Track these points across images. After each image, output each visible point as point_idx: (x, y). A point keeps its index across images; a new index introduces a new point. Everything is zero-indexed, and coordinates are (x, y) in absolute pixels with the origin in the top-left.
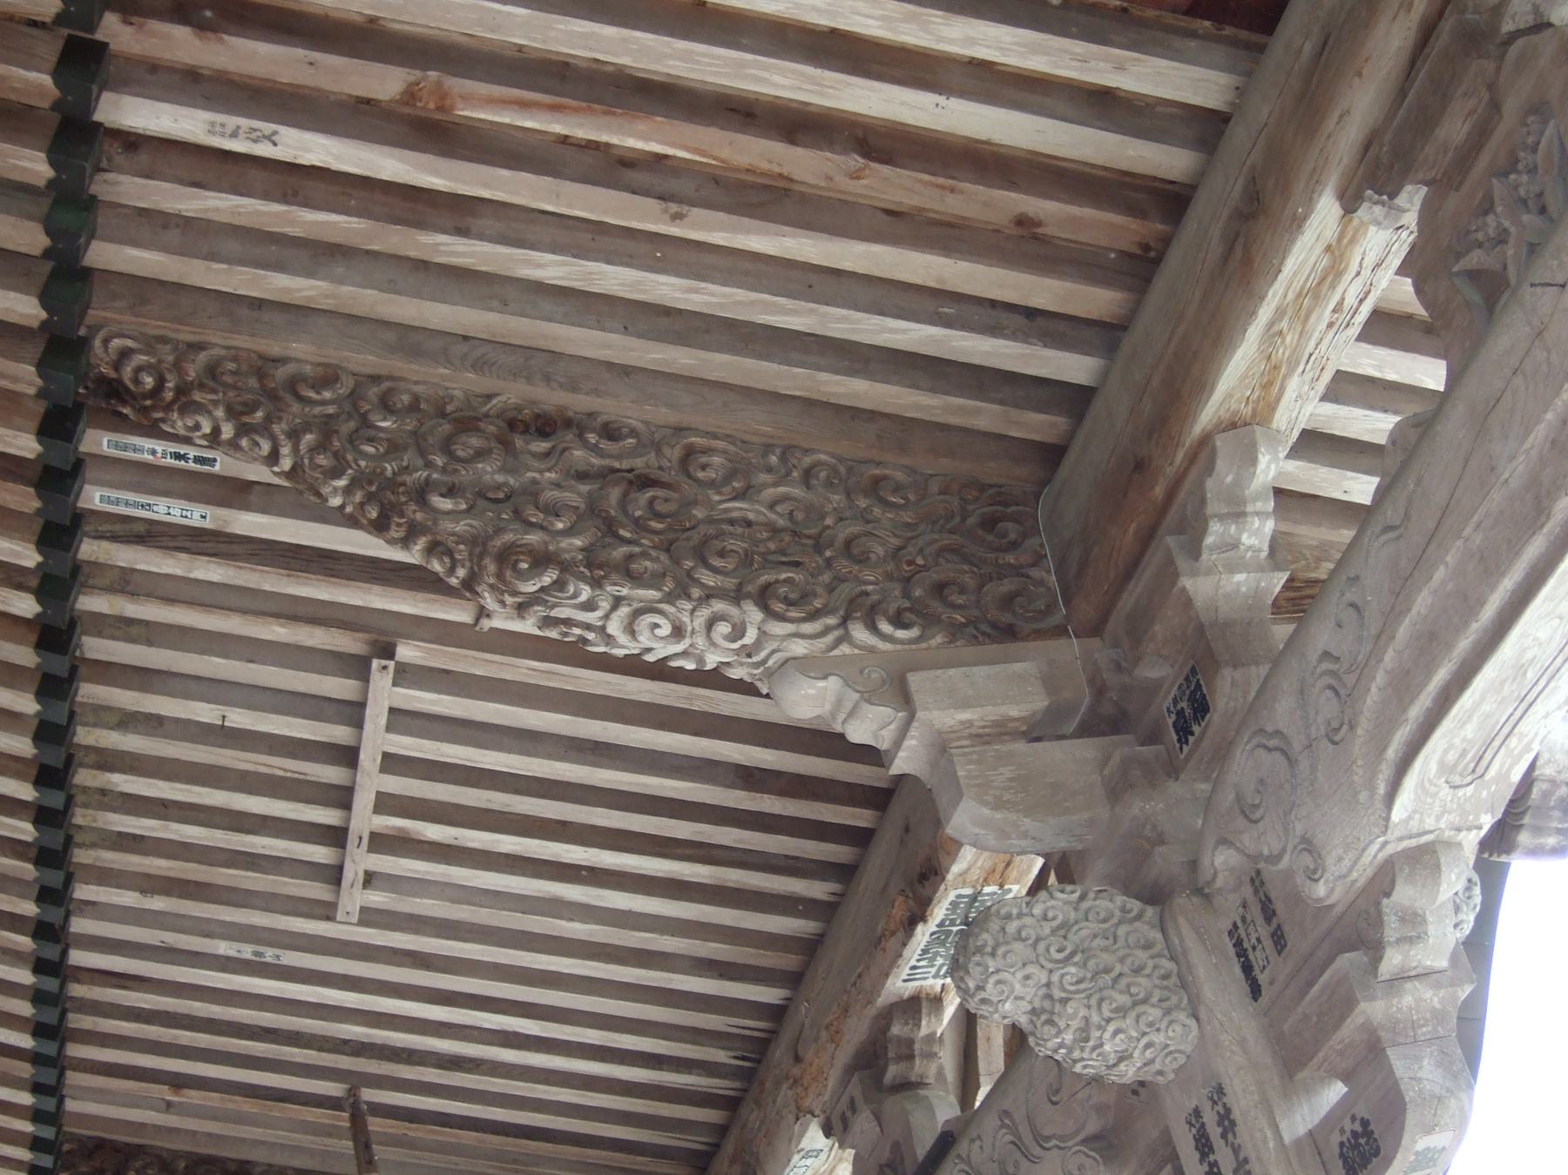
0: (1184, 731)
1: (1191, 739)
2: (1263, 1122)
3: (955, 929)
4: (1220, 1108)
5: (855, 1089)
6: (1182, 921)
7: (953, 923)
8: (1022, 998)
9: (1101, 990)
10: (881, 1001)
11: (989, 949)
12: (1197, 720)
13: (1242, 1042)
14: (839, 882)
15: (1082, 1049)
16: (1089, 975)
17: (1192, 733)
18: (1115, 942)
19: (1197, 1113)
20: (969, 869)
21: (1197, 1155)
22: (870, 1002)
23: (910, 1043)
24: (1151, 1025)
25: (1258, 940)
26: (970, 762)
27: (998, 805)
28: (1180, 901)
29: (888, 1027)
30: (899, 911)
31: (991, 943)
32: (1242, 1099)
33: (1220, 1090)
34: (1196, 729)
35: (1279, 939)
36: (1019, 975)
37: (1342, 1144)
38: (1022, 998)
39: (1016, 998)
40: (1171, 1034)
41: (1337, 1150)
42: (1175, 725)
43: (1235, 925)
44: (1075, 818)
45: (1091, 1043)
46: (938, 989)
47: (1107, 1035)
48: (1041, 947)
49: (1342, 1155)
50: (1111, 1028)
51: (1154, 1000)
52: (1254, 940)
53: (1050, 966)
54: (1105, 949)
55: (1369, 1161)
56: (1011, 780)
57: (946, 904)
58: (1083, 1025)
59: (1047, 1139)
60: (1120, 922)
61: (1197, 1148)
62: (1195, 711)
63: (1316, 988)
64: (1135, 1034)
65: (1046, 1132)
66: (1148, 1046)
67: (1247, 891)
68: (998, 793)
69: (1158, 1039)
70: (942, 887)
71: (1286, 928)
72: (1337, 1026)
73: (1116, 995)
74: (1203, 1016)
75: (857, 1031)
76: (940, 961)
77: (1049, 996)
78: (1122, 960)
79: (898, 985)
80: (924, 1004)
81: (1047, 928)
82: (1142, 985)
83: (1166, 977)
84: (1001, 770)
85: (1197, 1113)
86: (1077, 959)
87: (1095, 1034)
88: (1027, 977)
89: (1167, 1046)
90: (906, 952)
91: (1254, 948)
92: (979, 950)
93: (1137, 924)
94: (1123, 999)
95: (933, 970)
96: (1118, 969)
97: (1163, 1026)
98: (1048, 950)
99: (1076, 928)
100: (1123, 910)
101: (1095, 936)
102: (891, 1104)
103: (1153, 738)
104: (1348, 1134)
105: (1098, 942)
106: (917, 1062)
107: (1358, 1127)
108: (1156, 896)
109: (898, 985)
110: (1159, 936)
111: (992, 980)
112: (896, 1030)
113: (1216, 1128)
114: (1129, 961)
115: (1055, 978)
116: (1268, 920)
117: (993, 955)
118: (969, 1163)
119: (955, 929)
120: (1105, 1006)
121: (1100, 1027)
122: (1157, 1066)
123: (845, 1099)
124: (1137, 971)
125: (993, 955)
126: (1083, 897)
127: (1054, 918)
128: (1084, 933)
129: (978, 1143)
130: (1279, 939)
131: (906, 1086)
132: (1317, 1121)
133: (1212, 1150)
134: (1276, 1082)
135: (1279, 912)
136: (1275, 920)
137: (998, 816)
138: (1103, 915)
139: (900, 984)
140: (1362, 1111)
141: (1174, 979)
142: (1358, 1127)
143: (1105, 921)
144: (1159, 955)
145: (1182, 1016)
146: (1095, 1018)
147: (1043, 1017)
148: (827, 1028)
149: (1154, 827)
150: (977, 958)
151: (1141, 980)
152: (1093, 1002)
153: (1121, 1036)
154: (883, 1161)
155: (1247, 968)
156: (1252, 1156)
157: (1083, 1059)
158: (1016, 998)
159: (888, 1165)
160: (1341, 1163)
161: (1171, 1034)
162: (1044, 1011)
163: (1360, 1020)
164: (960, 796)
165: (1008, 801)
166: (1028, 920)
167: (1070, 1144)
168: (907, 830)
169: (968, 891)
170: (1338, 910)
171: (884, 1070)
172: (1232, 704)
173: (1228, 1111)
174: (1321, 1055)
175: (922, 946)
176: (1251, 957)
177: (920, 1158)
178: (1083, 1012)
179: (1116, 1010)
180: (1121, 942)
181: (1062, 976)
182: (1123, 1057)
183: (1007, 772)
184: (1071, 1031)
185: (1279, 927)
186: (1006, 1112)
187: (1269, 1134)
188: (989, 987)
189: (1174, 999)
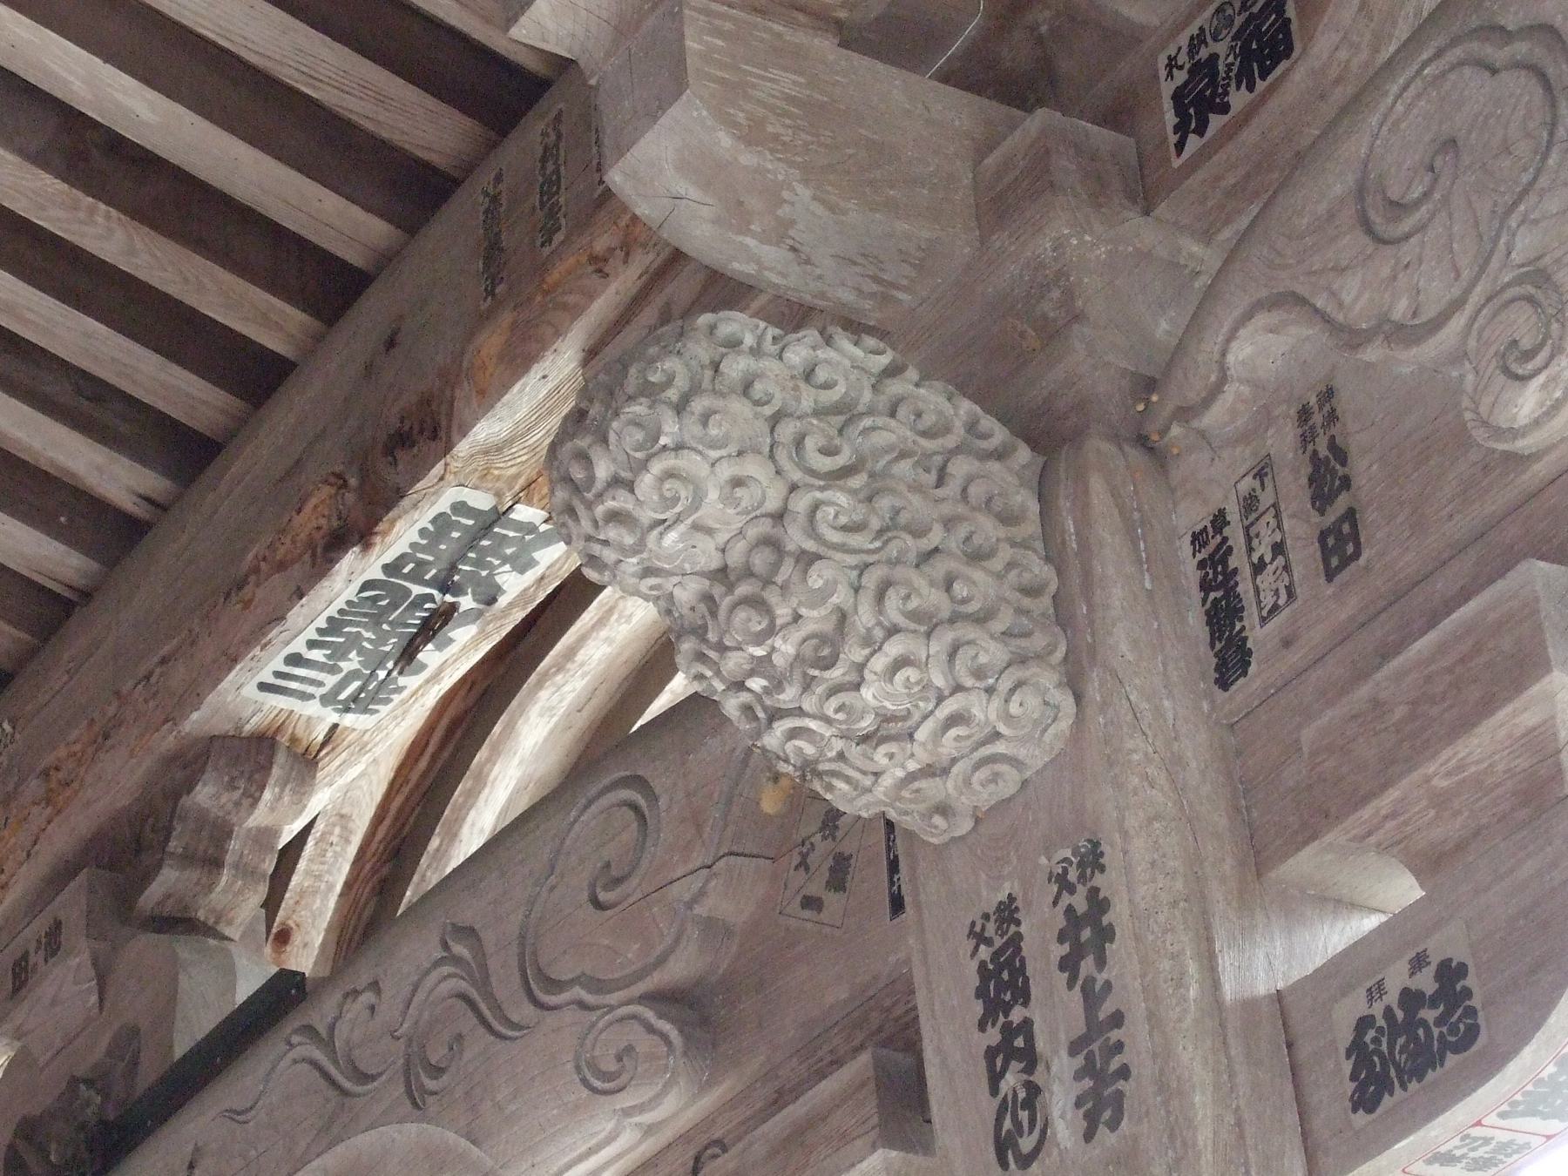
0: (1199, 102)
1: (1216, 122)
2: (1184, 941)
3: (417, 590)
4: (1079, 902)
5: (72, 904)
6: (1097, 484)
7: (416, 577)
8: (709, 531)
9: (894, 563)
10: (197, 721)
11: (672, 394)
12: (1246, 78)
13: (1174, 764)
14: (166, 472)
15: (808, 685)
16: (875, 524)
17: (1225, 109)
18: (940, 483)
19: (1007, 913)
20: (509, 442)
21: (978, 1008)
22: (171, 719)
23: (222, 832)
24: (979, 673)
25: (1278, 549)
26: (718, 33)
27: (752, 135)
28: (1097, 446)
29: (189, 785)
30: (313, 518)
31: (681, 383)
32: (1139, 885)
33: (1092, 860)
34: (1238, 99)
35: (1340, 547)
36: (726, 471)
37: (1364, 1023)
38: (709, 531)
39: (696, 527)
40: (1014, 708)
41: (1345, 1036)
42: (1177, 96)
43: (1220, 521)
44: (902, 226)
45: (836, 674)
46: (320, 734)
47: (879, 663)
48: (787, 430)
49: (1357, 1049)
50: (894, 648)
51: (998, 626)
52: (1263, 549)
53: (796, 476)
54: (916, 488)
55: (1436, 1060)
56: (790, 99)
57: (424, 518)
58: (828, 627)
59: (555, 985)
60: (957, 451)
61: (981, 993)
62: (1246, 55)
63: (1396, 663)
64: (939, 681)
65: (562, 971)
66: (954, 720)
67: (1282, 441)
68: (761, 112)
69: (983, 710)
70: (438, 469)
71: (1369, 518)
72: (1464, 725)
73: (920, 582)
74: (1093, 692)
75: (116, 783)
76: (352, 663)
77: (772, 543)
78: (949, 523)
79: (246, 695)
80: (281, 758)
81: (808, 399)
82: (978, 585)
83: (1032, 591)
84: (775, 73)
85: (1007, 913)
86: (857, 481)
87: (854, 653)
88: (738, 482)
89: (997, 735)
90: (296, 615)
91: (1259, 568)
92: (650, 391)
93: (994, 466)
94: (932, 598)
95: (330, 681)
96: (936, 537)
97: (1005, 684)
98: (799, 443)
99: (867, 422)
100: (972, 427)
101: (903, 455)
102: (144, 947)
103: (1118, 115)
104: (1392, 998)
105: (904, 467)
106: (225, 876)
107: (1426, 982)
108: (1048, 435)
109: (246, 695)
110: (1034, 507)
111: (657, 467)
112: (206, 794)
113: (1047, 953)
114: (962, 531)
115: (801, 504)
116: (1321, 498)
117: (680, 408)
118: (328, 1044)
119: (417, 590)
120: (893, 601)
121: (867, 641)
122: (946, 788)
123: (41, 925)
124: (976, 557)
125: (680, 408)
126: (892, 371)
127: (827, 386)
128: (881, 439)
129: (368, 997)
130: (1340, 547)
131: (179, 922)
132: (1296, 975)
133: (1024, 996)
134: (1228, 866)
135: (1359, 481)
136: (1342, 502)
137: (748, 159)
138: (929, 420)
139: (250, 690)
140: (1449, 944)
141: (1046, 602)
142: (1426, 982)
143: (925, 434)
144: (1024, 545)
145: (1048, 679)
146: (865, 617)
147: (743, 589)
148: (46, 774)
149: (1069, 295)
150: (638, 409)
151: (978, 575)
152: (871, 580)
153: (910, 673)
154: (81, 1071)
155: (1223, 617)
156: (1137, 1012)
157: (800, 712)
158: (696, 527)
159: (89, 1083)
160: (1347, 1067)
161: (1014, 708)
162: (748, 573)
163: (1529, 719)
164: (679, 84)
165: (776, 137)
166: (769, 365)
167: (613, 998)
168: (391, 343)
169: (482, 501)
170: (1540, 470)
171: (147, 877)
172: (1343, 54)
173: (1099, 905)
174: (1394, 794)
175: (332, 611)
176: (1244, 587)
177: (179, 1051)
178: (842, 597)
179: (914, 616)
180: (952, 489)
181: (816, 506)
182: (890, 729)
183: (788, 82)
184: (797, 635)
185: (1350, 515)
186: (468, 933)
187: (1192, 968)
188: (646, 482)
189: (1039, 641)
